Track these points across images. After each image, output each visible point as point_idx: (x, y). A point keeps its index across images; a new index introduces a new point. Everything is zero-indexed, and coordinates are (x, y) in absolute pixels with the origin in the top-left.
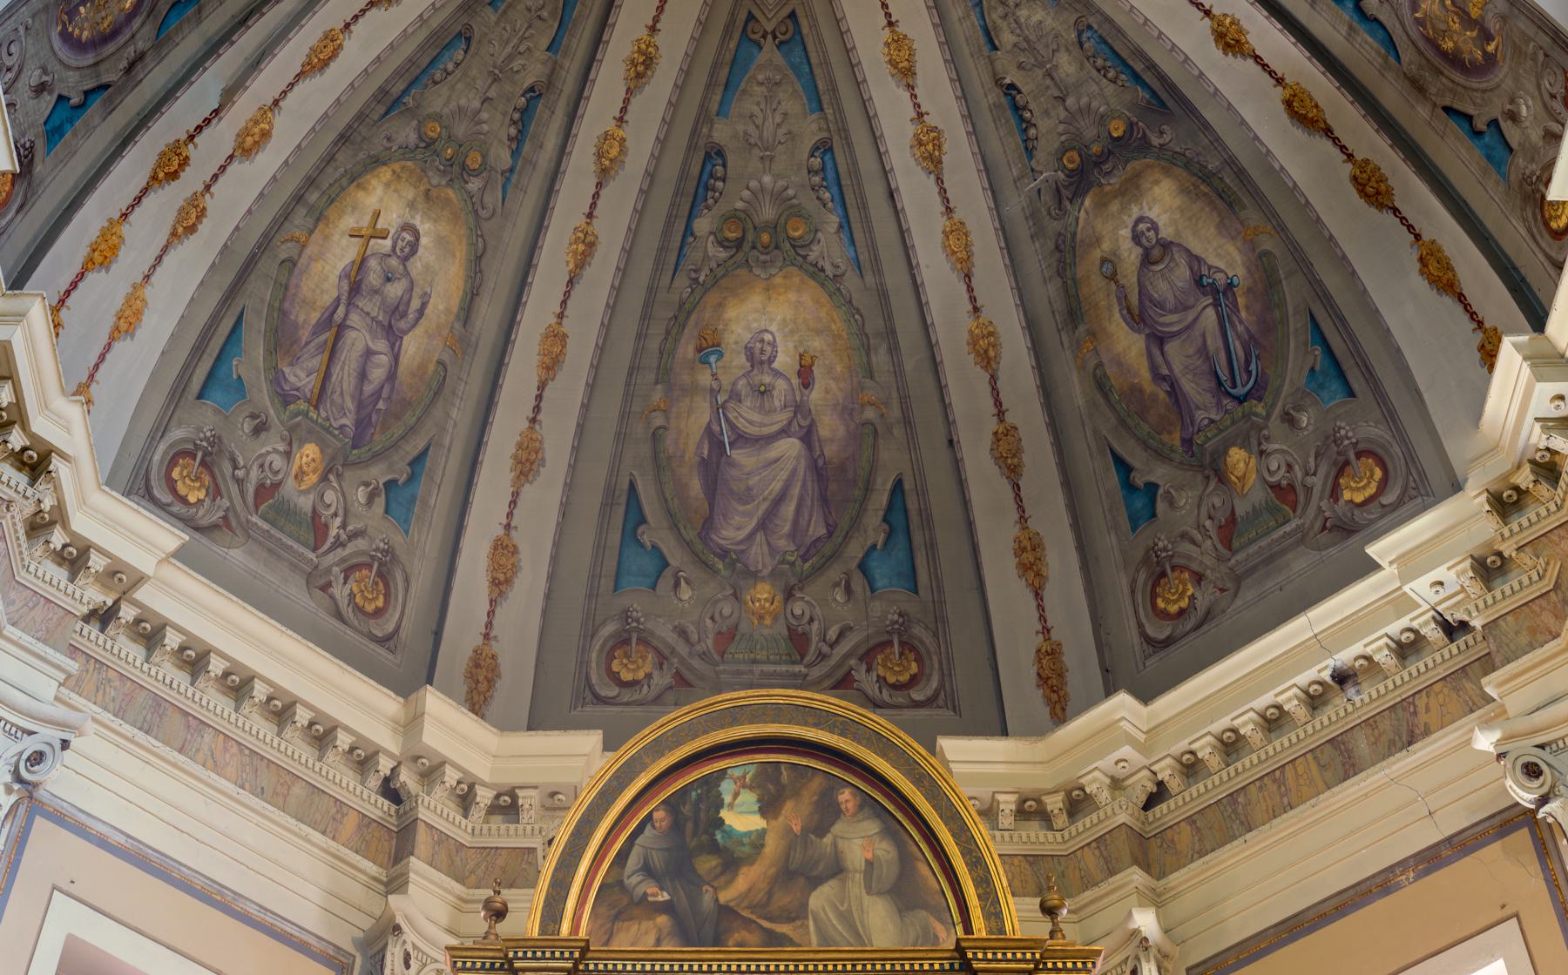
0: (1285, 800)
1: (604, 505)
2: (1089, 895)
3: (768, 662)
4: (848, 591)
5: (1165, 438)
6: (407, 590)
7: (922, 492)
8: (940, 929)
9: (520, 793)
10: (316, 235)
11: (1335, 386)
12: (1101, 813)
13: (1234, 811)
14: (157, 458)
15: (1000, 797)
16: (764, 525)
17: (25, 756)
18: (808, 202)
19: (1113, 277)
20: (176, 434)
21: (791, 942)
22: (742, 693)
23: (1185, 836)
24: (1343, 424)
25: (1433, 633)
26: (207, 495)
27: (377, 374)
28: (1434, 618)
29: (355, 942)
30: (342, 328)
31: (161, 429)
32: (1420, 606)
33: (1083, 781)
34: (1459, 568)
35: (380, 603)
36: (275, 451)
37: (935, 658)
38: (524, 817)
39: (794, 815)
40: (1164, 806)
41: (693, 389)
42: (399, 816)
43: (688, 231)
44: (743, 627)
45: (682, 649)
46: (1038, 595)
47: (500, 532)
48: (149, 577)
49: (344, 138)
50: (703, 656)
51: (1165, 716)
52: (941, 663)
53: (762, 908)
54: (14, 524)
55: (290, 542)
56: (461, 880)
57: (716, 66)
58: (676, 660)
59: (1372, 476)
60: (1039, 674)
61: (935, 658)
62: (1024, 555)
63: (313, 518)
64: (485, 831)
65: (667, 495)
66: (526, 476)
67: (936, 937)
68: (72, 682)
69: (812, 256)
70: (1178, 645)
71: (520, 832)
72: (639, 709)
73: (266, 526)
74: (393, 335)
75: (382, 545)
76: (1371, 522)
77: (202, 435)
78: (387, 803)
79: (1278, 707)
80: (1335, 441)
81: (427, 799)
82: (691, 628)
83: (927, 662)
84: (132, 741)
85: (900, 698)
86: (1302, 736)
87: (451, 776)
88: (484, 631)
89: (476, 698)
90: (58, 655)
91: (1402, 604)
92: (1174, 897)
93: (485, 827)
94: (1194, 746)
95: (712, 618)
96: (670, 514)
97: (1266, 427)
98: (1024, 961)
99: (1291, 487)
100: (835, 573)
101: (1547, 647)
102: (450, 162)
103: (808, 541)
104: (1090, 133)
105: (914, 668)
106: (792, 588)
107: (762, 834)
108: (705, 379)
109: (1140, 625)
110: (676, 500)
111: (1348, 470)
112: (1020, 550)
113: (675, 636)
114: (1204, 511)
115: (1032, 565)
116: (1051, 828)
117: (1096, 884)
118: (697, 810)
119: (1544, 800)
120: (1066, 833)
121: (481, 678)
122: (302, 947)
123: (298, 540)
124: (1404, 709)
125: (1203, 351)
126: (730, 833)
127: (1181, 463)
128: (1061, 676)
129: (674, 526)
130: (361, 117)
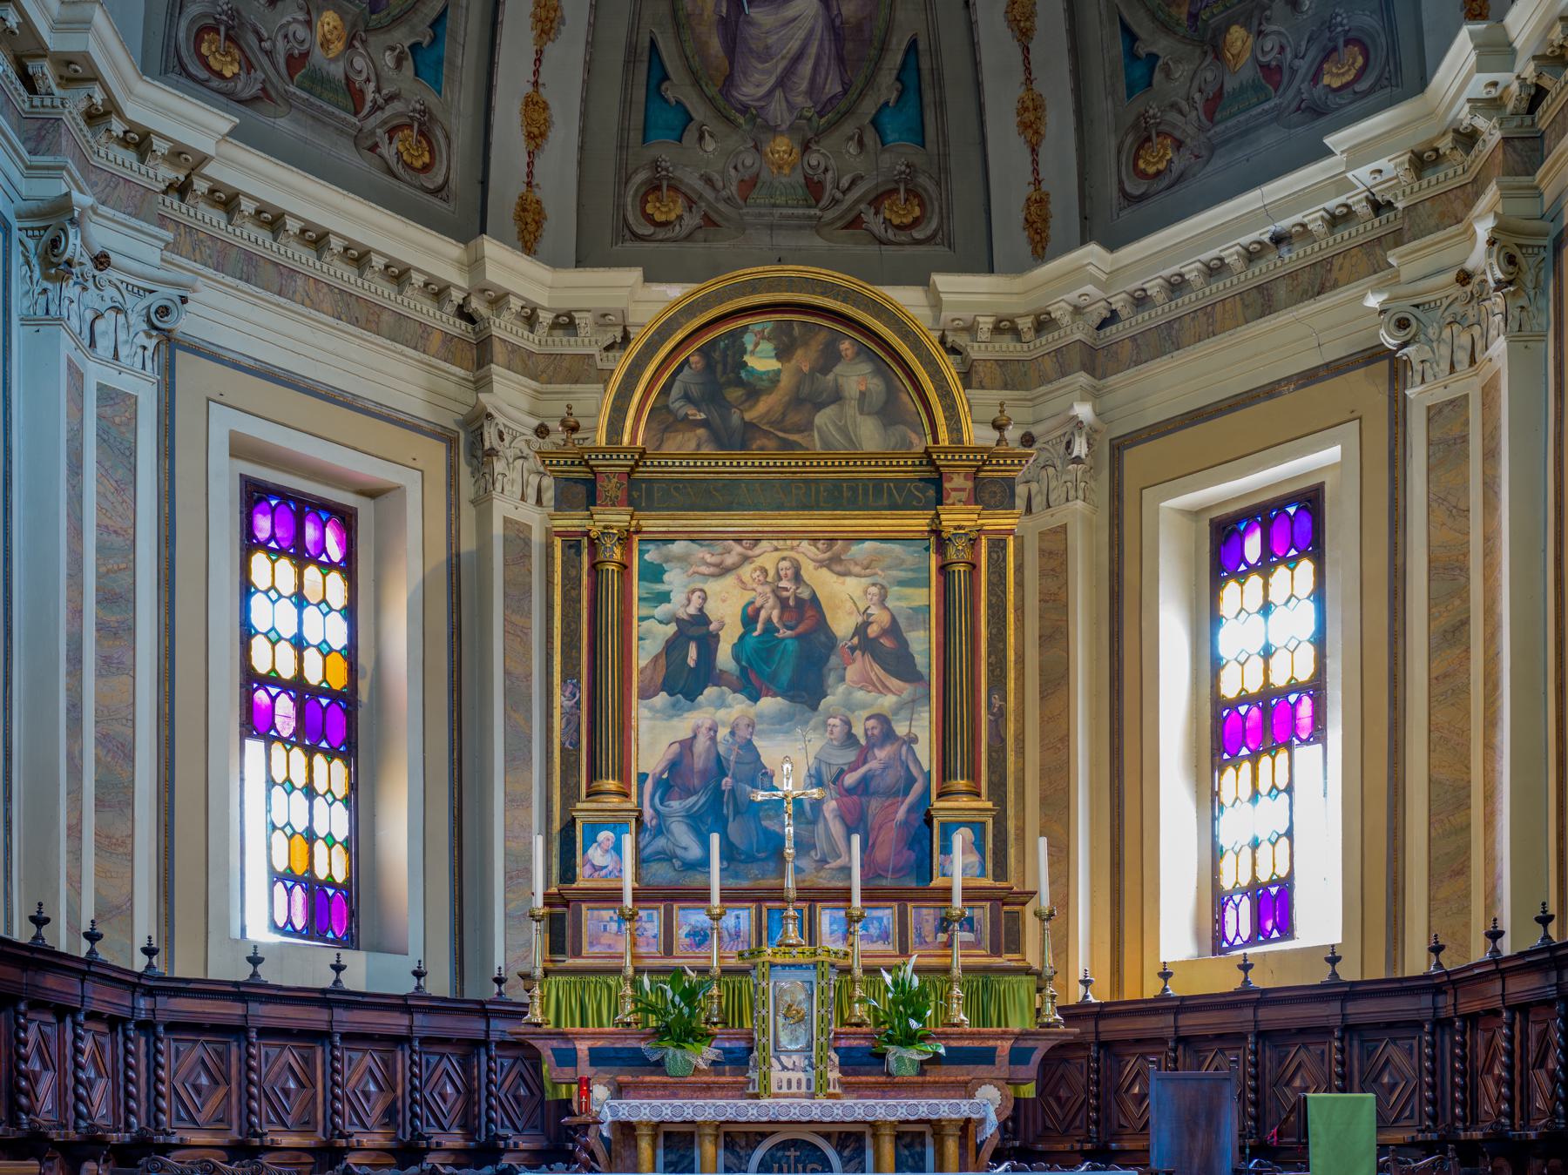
0: (1211, 329)
1: (627, 62)
2: (1043, 389)
3: (786, 206)
4: (861, 143)
5: (1174, 11)
6: (449, 146)
7: (935, 52)
8: (914, 438)
9: (576, 315)
12: (1062, 332)
13: (1169, 335)
14: (182, 35)
15: (980, 319)
16: (782, 82)
17: (153, 310)
21: (801, 447)
22: (760, 269)
24: (1341, 11)
25: (1362, 209)
26: (240, 68)
28: (1367, 197)
29: (457, 422)
32: (1357, 188)
33: (1050, 309)
34: (1398, 160)
35: (426, 158)
36: (295, 20)
37: (936, 204)
38: (582, 332)
39: (804, 359)
40: (1114, 328)
42: (475, 333)
44: (764, 175)
45: (709, 194)
46: (1034, 151)
47: (530, 89)
48: (212, 158)
51: (1126, 262)
52: (941, 208)
53: (779, 423)
54: (74, 119)
55: (331, 109)
56: (535, 378)
58: (703, 204)
59: (1353, 63)
60: (1026, 220)
61: (936, 204)
62: (1026, 115)
63: (348, 85)
64: (550, 342)
65: (688, 52)
66: (548, 34)
67: (911, 443)
68: (171, 246)
70: (1150, 200)
71: (580, 342)
72: (674, 244)
73: (305, 95)
75: (418, 106)
76: (1342, 106)
77: (219, 9)
78: (463, 323)
79: (1221, 259)
80: (1329, 28)
81: (497, 321)
82: (716, 176)
83: (929, 208)
84: (236, 289)
85: (903, 237)
86: (1235, 282)
87: (516, 304)
88: (526, 180)
89: (527, 238)
90: (152, 227)
91: (1342, 185)
92: (1110, 392)
93: (550, 339)
94: (1145, 286)
95: (735, 168)
96: (692, 73)
97: (1269, 7)
98: (975, 460)
99: (1279, 68)
100: (849, 128)
101: (1448, 230)
103: (824, 98)
105: (917, 212)
106: (809, 141)
107: (778, 372)
109: (1121, 182)
110: (697, 58)
111: (1335, 56)
113: (702, 183)
114: (1196, 84)
115: (1032, 123)
116: (1020, 340)
117: (1050, 382)
118: (725, 356)
119: (1404, 345)
120: (1031, 345)
121: (529, 220)
123: (337, 106)
124: (1322, 267)
126: (752, 372)
127: (1184, 37)
128: (1045, 220)
129: (696, 82)
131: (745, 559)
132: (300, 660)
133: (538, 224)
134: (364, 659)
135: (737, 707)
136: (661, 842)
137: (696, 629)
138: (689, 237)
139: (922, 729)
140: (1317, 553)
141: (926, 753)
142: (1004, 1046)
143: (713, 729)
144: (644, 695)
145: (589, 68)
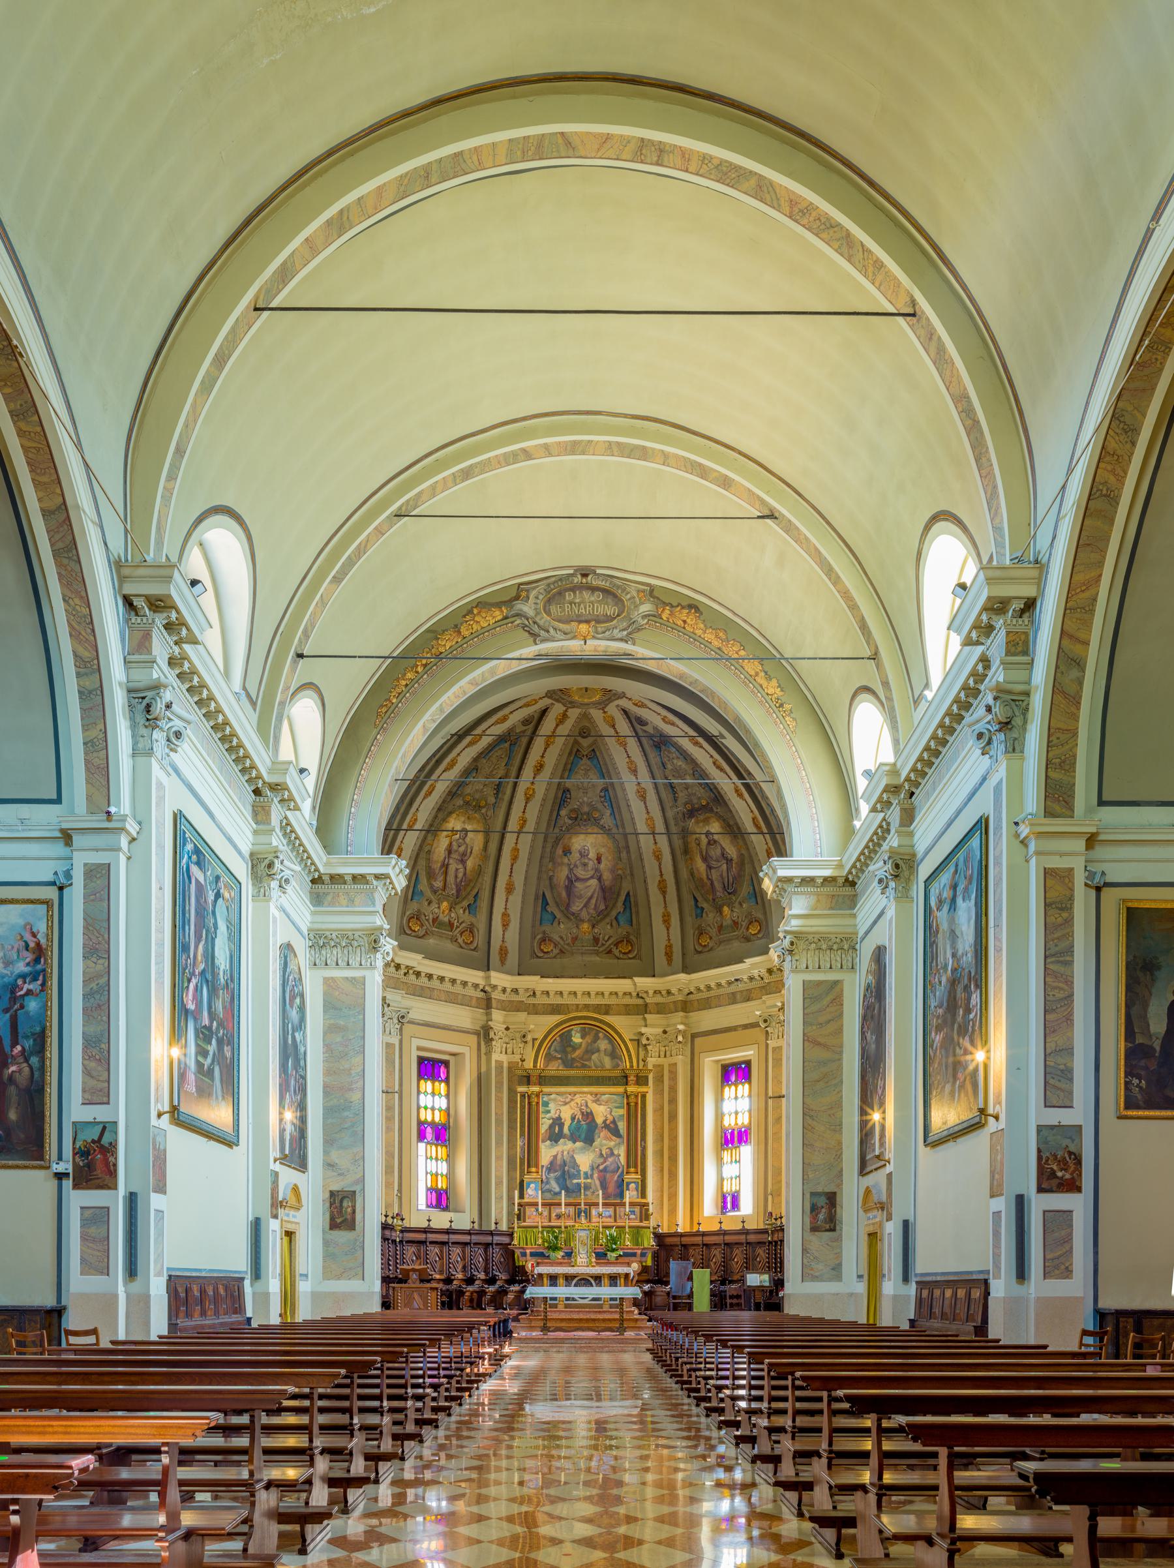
4: (611, 925)
7: (635, 896)
10: (436, 841)
11: (754, 899)
16: (586, 906)
18: (600, 806)
19: (699, 845)
20: (408, 913)
23: (696, 1004)
27: (460, 875)
30: (448, 865)
31: (404, 913)
39: (589, 1039)
41: (563, 864)
43: (558, 814)
45: (562, 942)
46: (668, 929)
49: (439, 809)
50: (568, 944)
53: (582, 1058)
57: (566, 764)
69: (601, 823)
74: (463, 862)
85: (625, 957)
87: (500, 988)
96: (556, 903)
100: (608, 920)
102: (475, 806)
104: (695, 801)
108: (566, 860)
112: (664, 916)
122: (468, 1032)
125: (721, 876)
130: (444, 802)
131: (572, 1100)
132: (433, 1114)
133: (506, 954)
134: (452, 1112)
135: (570, 1145)
136: (548, 1186)
137: (558, 1122)
138: (555, 957)
139: (621, 1151)
140: (750, 1083)
141: (623, 1160)
142: (639, 1252)
143: (563, 1152)
144: (543, 1141)
145: (523, 902)
